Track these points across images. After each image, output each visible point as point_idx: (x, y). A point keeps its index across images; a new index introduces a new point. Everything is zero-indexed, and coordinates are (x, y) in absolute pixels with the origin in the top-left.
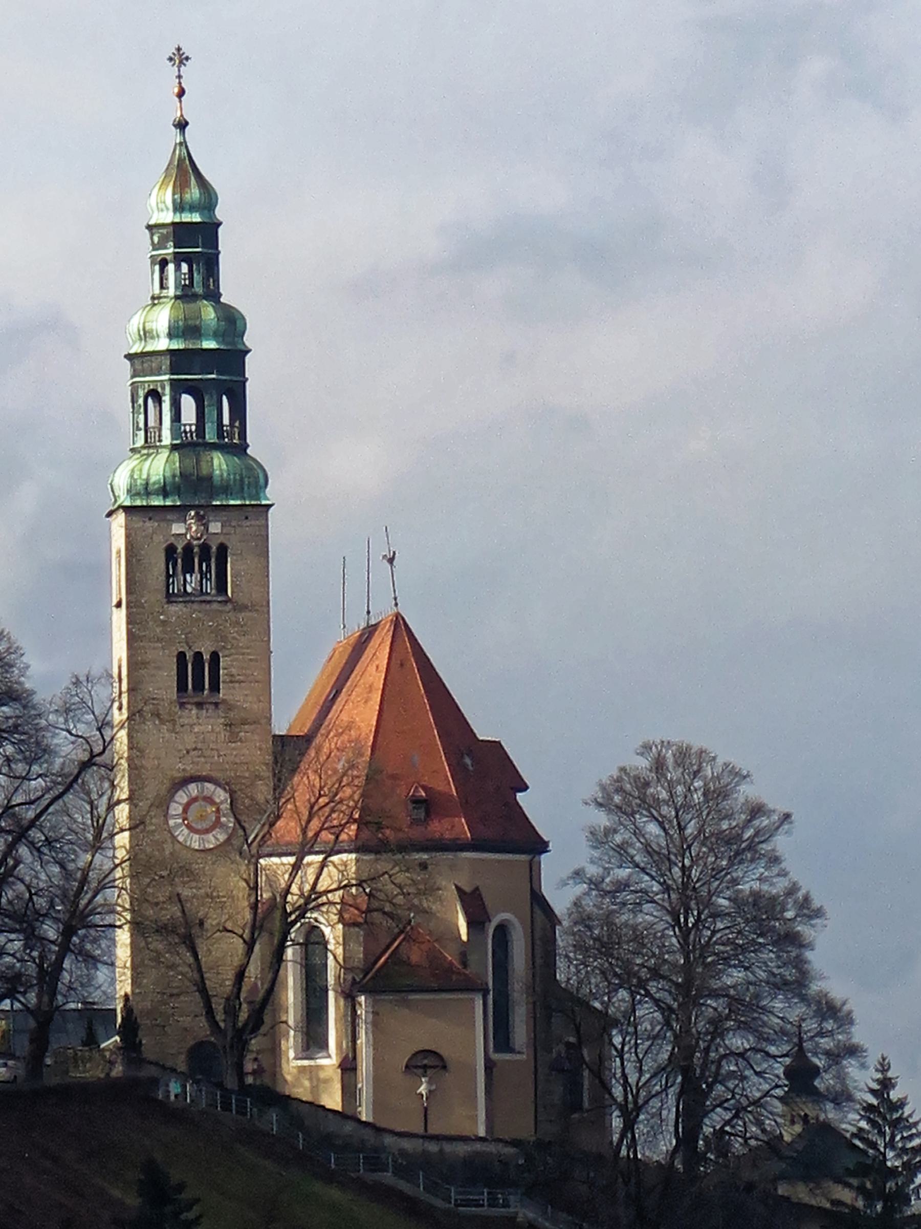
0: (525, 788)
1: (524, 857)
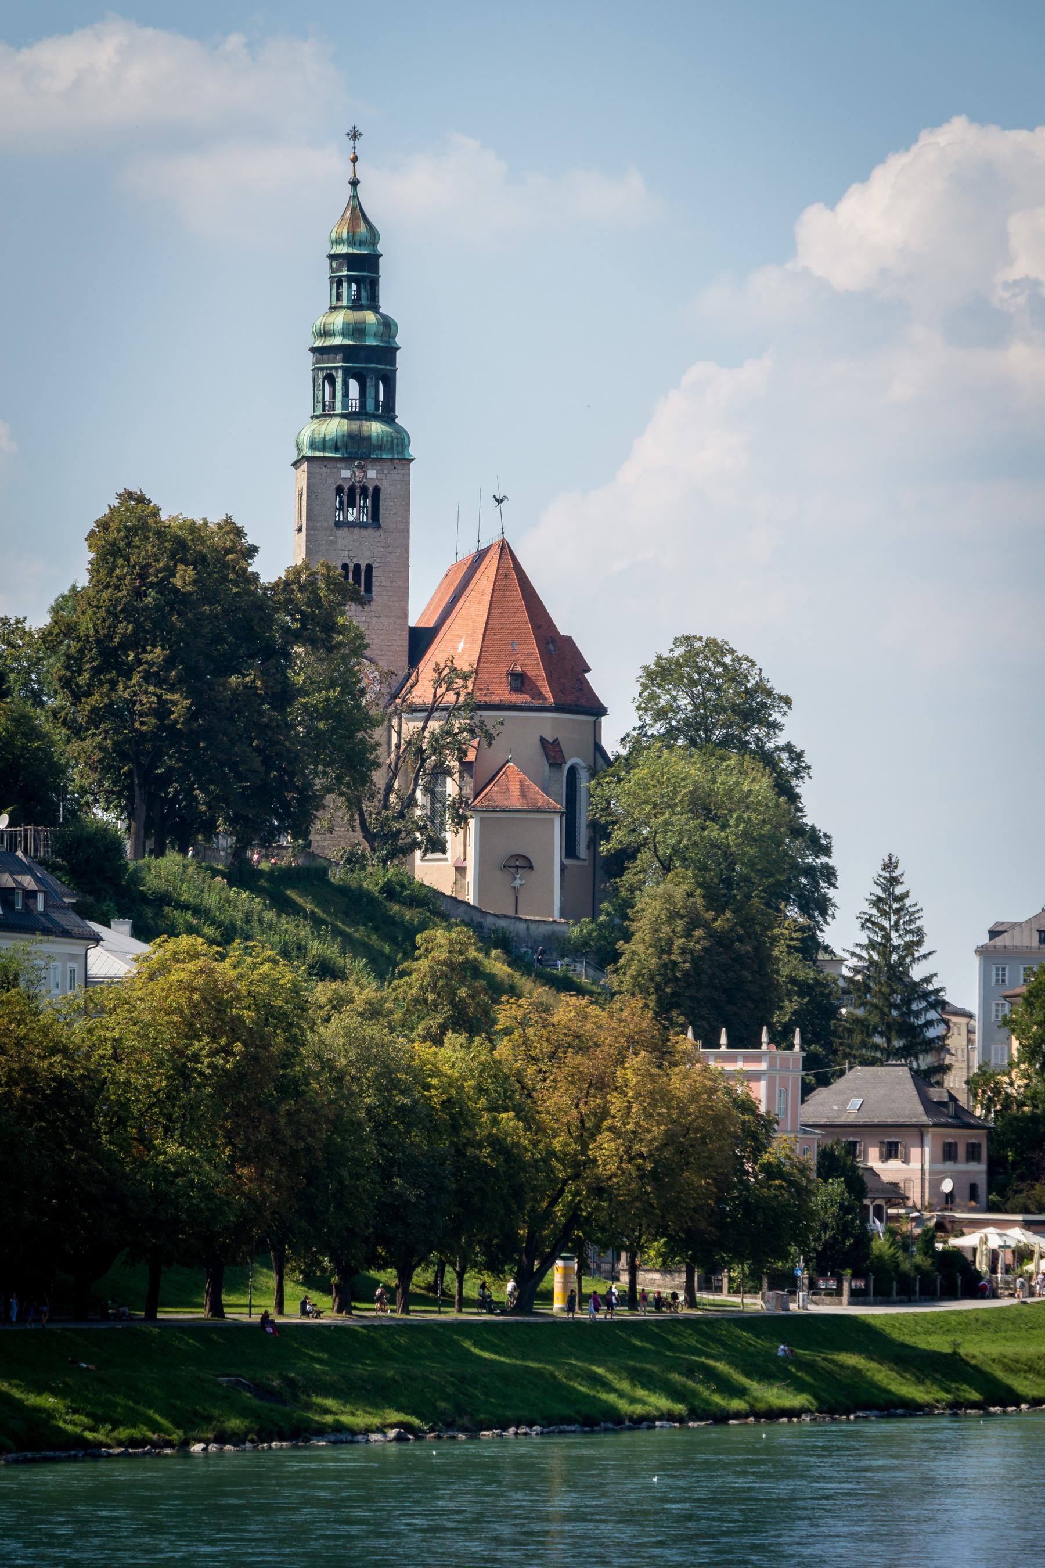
0: (588, 670)
1: (591, 718)
